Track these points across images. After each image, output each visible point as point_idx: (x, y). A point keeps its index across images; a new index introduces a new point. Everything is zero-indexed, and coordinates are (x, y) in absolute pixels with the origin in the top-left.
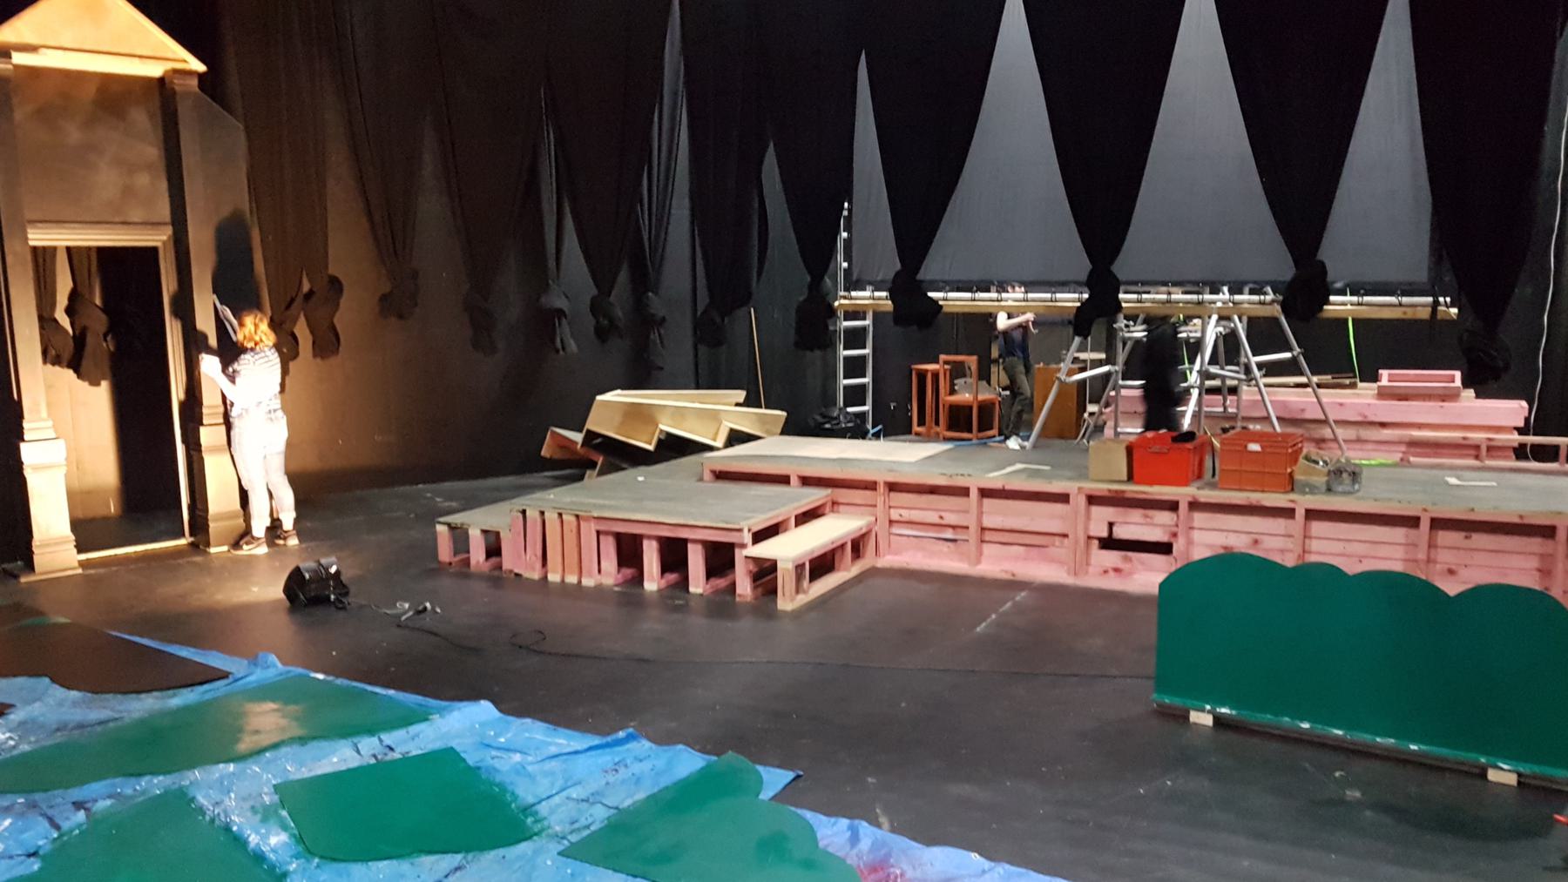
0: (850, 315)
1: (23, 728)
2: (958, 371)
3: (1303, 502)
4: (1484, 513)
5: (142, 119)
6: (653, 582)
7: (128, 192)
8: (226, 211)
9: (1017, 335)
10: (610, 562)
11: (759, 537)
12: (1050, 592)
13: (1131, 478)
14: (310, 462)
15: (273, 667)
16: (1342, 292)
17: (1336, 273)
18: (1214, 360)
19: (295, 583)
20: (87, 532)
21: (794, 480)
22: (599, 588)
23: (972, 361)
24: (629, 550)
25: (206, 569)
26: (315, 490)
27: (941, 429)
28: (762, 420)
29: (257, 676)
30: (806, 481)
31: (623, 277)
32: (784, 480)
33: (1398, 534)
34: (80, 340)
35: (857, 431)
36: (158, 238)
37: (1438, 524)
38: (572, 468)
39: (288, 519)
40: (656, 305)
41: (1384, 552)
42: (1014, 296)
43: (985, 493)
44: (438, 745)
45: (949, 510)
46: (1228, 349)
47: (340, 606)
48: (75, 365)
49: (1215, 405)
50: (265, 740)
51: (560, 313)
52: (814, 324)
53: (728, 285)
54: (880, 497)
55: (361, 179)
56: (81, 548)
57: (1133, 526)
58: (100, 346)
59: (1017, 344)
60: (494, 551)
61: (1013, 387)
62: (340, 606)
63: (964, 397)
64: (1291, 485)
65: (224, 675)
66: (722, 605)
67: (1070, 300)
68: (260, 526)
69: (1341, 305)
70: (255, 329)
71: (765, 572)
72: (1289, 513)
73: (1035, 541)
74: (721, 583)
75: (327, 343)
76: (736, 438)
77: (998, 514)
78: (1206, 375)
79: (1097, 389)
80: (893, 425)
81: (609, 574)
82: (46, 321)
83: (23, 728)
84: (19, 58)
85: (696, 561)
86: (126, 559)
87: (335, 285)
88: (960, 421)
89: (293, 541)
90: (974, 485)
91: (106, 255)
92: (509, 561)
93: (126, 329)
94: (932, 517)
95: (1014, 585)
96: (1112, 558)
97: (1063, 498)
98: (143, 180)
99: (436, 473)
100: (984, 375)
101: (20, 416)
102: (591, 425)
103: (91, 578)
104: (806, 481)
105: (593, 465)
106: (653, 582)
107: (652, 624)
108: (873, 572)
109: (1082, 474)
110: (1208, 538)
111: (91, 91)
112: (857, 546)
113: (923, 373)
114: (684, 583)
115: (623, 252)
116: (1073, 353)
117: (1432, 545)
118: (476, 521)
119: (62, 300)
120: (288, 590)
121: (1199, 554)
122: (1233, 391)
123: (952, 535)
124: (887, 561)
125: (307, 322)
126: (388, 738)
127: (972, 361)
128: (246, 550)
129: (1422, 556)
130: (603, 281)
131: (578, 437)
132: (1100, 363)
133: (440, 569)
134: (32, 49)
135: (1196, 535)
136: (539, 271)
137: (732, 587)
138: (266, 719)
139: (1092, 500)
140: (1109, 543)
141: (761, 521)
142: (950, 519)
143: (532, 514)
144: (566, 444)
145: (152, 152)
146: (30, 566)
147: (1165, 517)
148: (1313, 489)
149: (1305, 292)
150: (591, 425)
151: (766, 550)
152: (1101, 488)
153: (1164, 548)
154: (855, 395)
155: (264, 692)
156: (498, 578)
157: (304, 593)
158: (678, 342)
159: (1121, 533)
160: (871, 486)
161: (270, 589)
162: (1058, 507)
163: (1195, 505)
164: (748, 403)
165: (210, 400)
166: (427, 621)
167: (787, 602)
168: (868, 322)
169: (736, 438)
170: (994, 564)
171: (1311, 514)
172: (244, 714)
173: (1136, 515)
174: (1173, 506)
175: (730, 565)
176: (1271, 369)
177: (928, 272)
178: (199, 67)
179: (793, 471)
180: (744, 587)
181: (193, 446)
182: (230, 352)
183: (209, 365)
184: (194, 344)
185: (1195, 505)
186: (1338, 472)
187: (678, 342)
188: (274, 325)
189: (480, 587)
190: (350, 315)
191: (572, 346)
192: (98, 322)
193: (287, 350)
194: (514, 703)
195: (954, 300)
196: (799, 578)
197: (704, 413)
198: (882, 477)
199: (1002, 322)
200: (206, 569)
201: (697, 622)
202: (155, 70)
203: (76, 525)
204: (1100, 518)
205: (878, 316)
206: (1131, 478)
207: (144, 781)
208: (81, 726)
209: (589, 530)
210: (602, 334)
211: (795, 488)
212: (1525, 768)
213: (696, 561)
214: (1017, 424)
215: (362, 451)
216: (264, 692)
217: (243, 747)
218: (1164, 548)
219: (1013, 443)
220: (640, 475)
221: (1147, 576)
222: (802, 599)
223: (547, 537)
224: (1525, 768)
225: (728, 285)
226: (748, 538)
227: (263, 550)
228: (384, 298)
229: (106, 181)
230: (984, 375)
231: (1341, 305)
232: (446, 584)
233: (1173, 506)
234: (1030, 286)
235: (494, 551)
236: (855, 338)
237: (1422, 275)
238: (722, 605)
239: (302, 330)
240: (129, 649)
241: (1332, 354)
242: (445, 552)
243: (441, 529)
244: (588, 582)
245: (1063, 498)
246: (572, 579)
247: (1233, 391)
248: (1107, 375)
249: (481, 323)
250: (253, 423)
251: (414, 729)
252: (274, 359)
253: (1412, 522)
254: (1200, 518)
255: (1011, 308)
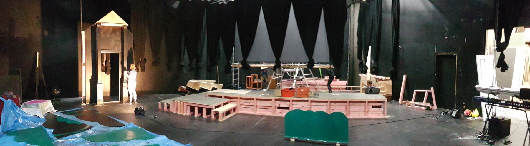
0: (235, 68)
1: (94, 131)
2: (254, 77)
3: (310, 99)
4: (337, 100)
5: (118, 33)
6: (196, 115)
7: (115, 45)
8: (129, 48)
9: (265, 71)
10: (189, 111)
11: (216, 107)
12: (269, 117)
13: (282, 96)
14: (139, 90)
15: (132, 125)
16: (318, 64)
17: (316, 61)
18: (298, 75)
19: (136, 110)
20: (105, 99)
21: (223, 97)
22: (187, 116)
23: (257, 75)
24: (192, 109)
25: (122, 106)
26: (140, 94)
27: (252, 88)
28: (218, 86)
29: (130, 126)
30: (226, 97)
31: (194, 60)
32: (221, 97)
33: (325, 104)
34: (106, 68)
35: (236, 88)
36: (119, 52)
37: (331, 102)
38: (183, 93)
39: (135, 100)
40: (200, 65)
41: (323, 108)
42: (264, 64)
43: (257, 99)
44: (157, 143)
45: (251, 103)
46: (300, 73)
47: (143, 115)
48: (105, 72)
49: (299, 82)
50: (130, 138)
51: (183, 66)
52: (228, 69)
53: (213, 61)
54: (238, 100)
55: (151, 41)
56: (104, 101)
57: (283, 105)
58: (109, 69)
59: (265, 72)
60: (168, 107)
61: (264, 80)
62: (143, 115)
63: (256, 82)
64: (308, 96)
65: (125, 125)
66: (209, 120)
67: (273, 65)
68: (131, 100)
69: (316, 66)
70: (133, 66)
71: (217, 114)
72: (307, 101)
73: (266, 108)
74: (209, 116)
75: (143, 70)
76: (214, 89)
77: (260, 103)
78: (296, 78)
79: (279, 80)
80: (243, 87)
81: (188, 113)
82: (102, 65)
83: (94, 131)
84: (102, 24)
85: (204, 111)
86: (110, 104)
87: (145, 59)
88: (255, 86)
89: (136, 103)
90: (255, 98)
91: (111, 54)
92: (171, 110)
93: (113, 66)
94: (248, 104)
95: (262, 116)
96: (280, 110)
97: (271, 100)
98: (118, 43)
99: (160, 93)
100: (259, 78)
101: (97, 79)
102: (188, 85)
103: (105, 106)
104: (226, 97)
105: (187, 93)
106: (196, 115)
107: (196, 123)
108: (237, 114)
109: (274, 95)
110: (295, 106)
111: (111, 29)
112: (234, 109)
113: (248, 78)
114: (202, 116)
115: (195, 55)
116: (274, 74)
117: (330, 105)
118: (166, 102)
119: (104, 62)
120: (135, 111)
121: (294, 109)
122: (302, 80)
123: (251, 107)
124: (240, 112)
125: (141, 67)
126: (148, 141)
127: (257, 75)
128: (128, 104)
129: (328, 107)
130: (191, 60)
131: (185, 88)
132: (279, 76)
133: (158, 110)
134: (104, 23)
135: (294, 106)
136: (180, 59)
137: (211, 117)
138: (130, 134)
139: (276, 100)
140: (279, 108)
141: (217, 105)
142: (251, 104)
143: (176, 101)
144: (182, 89)
145: (119, 38)
146: (96, 104)
147: (288, 103)
148: (311, 97)
149: (311, 64)
150: (188, 85)
151: (217, 110)
152: (277, 98)
153: (288, 108)
154: (236, 82)
155: (130, 129)
156: (169, 113)
157: (138, 112)
158: (204, 71)
159: (281, 106)
160: (237, 98)
161: (132, 111)
162: (270, 102)
163: (293, 101)
164: (216, 83)
165: (125, 78)
166: (156, 120)
167: (221, 120)
168: (238, 69)
169: (214, 89)
170: (259, 112)
171: (312, 101)
172: (127, 133)
173: (283, 103)
174: (289, 101)
175: (211, 113)
176: (307, 76)
177: (248, 60)
178: (127, 25)
179: (223, 95)
180: (213, 117)
181: (122, 86)
182: (129, 70)
183: (126, 72)
184: (123, 69)
185: (293, 101)
186: (315, 94)
187: (204, 71)
188: (136, 66)
189: (165, 114)
190: (147, 65)
191: (185, 72)
192: (109, 65)
193: (137, 70)
194: (170, 137)
195: (252, 65)
196: (223, 116)
197: (208, 84)
198: (239, 97)
199: (262, 68)
200: (122, 106)
201: (204, 123)
202: (121, 26)
203: (104, 97)
204: (277, 104)
205: (240, 68)
206: (282, 96)
207: (112, 143)
208: (103, 131)
209: (185, 105)
210: (190, 70)
211: (223, 99)
212: (341, 142)
213: (204, 111)
214: (265, 87)
215: (147, 88)
216: (130, 129)
217: (126, 139)
218: (288, 108)
219: (264, 90)
220: (195, 95)
221: (284, 113)
222: (224, 119)
223: (178, 105)
224: (341, 142)
225: (213, 61)
226: (214, 108)
227: (131, 104)
228: (153, 62)
229: (113, 43)
230: (259, 78)
231: (316, 66)
232: (159, 112)
233: (289, 101)
234: (267, 62)
235: (168, 107)
236: (236, 72)
237: (328, 61)
238: (209, 120)
239: (139, 67)
240: (110, 119)
241: (317, 74)
242: (160, 107)
243: (160, 103)
244: (184, 114)
245: (271, 100)
246: (182, 114)
247: (302, 80)
248: (281, 78)
249: (169, 67)
250: (132, 81)
251: (153, 139)
252: (136, 72)
253: (327, 102)
254: (294, 103)
255: (263, 66)
